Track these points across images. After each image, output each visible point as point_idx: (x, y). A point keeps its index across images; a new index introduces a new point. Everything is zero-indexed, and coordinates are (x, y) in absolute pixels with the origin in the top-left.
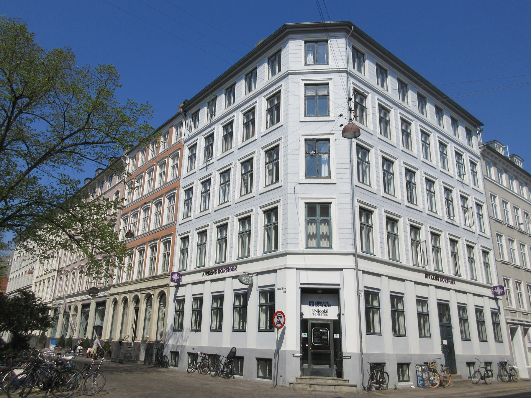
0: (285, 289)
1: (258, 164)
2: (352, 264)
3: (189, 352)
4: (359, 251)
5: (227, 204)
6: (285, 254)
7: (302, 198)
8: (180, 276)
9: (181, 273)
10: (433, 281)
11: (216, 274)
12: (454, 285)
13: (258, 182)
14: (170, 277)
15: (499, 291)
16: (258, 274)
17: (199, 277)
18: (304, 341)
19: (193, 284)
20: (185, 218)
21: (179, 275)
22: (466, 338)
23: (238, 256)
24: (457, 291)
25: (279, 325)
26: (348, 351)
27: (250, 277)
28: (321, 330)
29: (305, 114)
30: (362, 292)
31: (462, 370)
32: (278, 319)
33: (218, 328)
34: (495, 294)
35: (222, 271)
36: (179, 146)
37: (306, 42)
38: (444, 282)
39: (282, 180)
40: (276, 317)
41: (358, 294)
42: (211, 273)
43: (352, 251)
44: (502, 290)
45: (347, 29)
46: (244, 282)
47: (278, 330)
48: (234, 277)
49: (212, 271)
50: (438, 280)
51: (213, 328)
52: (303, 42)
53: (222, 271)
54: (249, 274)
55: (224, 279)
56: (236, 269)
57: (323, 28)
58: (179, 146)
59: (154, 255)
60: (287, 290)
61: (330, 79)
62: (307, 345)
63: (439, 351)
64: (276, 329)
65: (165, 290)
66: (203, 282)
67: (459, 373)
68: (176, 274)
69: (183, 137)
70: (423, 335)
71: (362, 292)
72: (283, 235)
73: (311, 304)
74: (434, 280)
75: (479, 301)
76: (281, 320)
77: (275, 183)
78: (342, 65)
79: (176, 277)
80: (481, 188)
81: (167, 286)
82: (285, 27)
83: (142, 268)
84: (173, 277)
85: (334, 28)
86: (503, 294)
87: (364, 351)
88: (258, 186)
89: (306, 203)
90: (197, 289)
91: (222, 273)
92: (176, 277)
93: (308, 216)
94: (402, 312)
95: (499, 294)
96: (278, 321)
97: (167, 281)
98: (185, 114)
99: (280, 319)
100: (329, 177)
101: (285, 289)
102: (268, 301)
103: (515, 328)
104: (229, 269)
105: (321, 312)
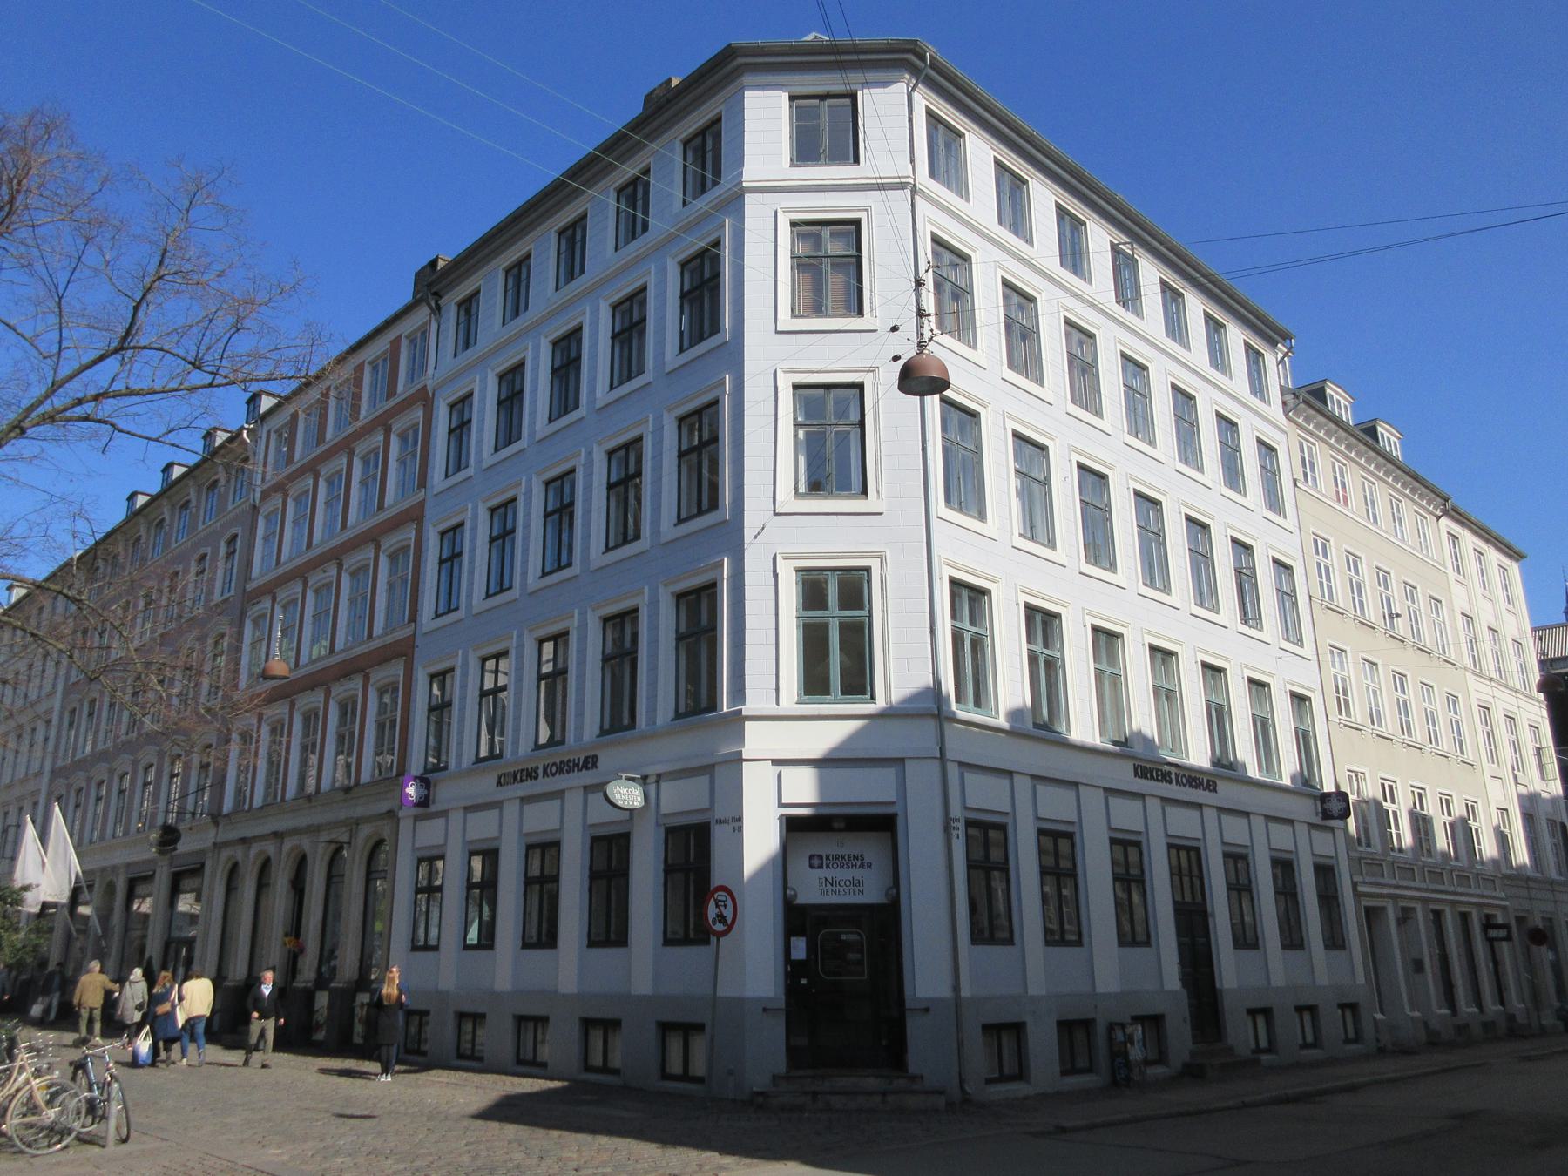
5: (565, 573)
10: (1156, 783)
11: (536, 778)
18: (793, 970)
20: (442, 615)
22: (1246, 939)
23: (601, 727)
24: (1221, 810)
25: (719, 927)
28: (844, 937)
29: (793, 310)
31: (1240, 1034)
33: (544, 938)
35: (554, 769)
37: (792, 98)
38: (1185, 786)
41: (947, 829)
47: (718, 940)
50: (1171, 782)
51: (419, 941)
52: (785, 96)
56: (595, 765)
57: (832, 58)
61: (867, 210)
62: (804, 981)
63: (1172, 978)
64: (713, 939)
73: (816, 862)
75: (1282, 838)
78: (896, 167)
82: (729, 53)
85: (862, 57)
87: (966, 992)
89: (798, 570)
90: (482, 827)
91: (554, 775)
93: (805, 608)
96: (718, 916)
99: (722, 908)
105: (842, 883)
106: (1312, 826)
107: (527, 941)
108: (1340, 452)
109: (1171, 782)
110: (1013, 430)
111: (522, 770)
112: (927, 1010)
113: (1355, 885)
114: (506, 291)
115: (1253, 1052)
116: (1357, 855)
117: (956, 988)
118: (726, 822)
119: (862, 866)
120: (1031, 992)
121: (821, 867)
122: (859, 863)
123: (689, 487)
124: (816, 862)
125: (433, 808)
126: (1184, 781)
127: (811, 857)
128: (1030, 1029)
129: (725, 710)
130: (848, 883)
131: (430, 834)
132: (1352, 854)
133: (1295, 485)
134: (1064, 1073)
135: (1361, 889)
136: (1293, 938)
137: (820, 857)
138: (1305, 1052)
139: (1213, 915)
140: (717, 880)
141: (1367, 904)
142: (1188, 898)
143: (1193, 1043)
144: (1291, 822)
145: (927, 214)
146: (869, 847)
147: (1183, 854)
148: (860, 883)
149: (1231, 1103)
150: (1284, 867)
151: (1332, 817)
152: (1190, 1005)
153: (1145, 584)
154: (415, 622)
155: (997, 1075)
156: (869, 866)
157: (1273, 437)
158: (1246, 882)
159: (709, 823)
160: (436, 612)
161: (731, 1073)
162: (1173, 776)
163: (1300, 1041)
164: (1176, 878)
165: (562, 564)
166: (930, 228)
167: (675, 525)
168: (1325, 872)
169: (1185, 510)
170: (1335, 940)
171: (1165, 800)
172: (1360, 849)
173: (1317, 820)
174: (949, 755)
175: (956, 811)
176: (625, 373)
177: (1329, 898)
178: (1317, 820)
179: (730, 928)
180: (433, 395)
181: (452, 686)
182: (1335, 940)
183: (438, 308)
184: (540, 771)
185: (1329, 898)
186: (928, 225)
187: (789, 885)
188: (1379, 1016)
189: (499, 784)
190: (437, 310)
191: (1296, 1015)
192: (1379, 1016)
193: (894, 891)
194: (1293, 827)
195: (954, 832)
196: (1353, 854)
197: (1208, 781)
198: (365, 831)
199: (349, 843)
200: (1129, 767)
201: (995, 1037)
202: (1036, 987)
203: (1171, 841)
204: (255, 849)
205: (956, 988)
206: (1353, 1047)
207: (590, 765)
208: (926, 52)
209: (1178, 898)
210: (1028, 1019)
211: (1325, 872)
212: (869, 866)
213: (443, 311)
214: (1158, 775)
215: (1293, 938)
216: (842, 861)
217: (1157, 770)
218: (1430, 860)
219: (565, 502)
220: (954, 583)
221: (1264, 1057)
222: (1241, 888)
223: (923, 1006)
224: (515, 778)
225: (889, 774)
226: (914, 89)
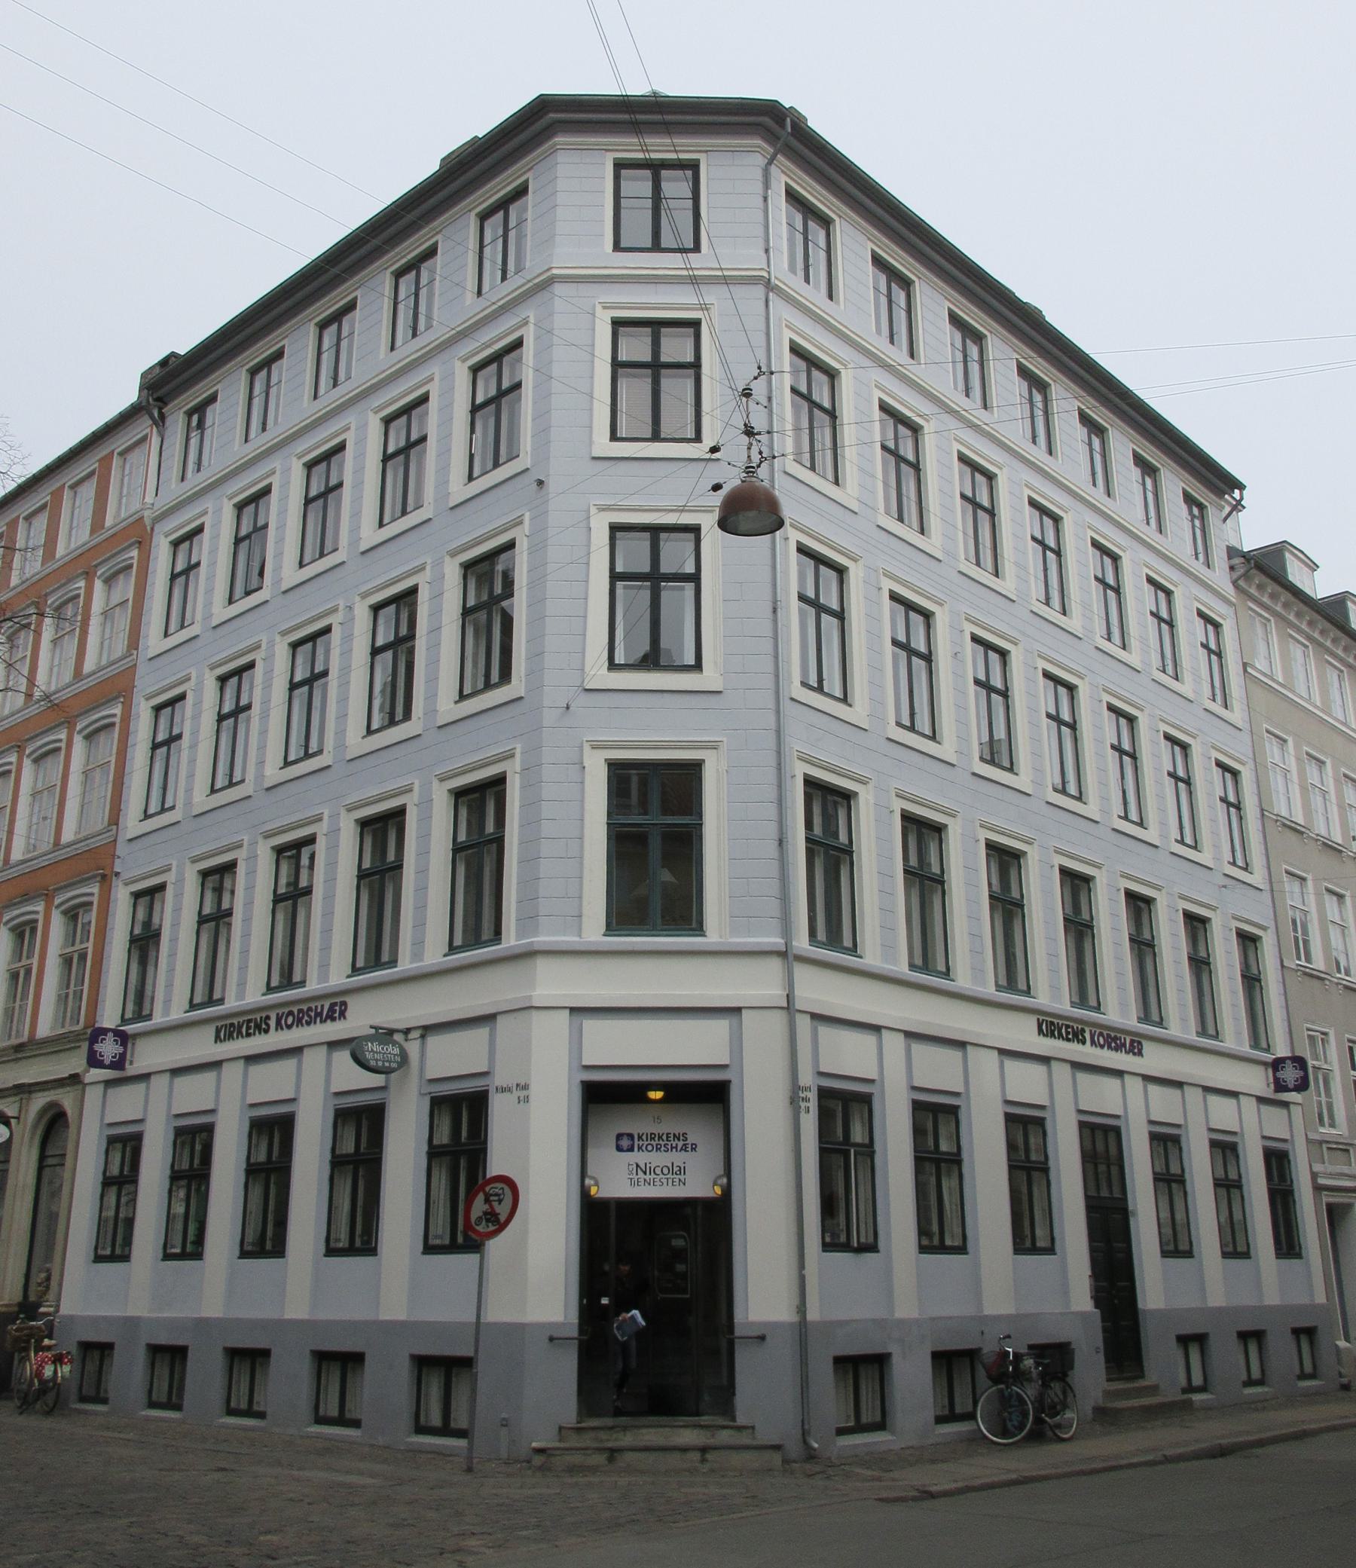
0: (526, 1087)
1: (436, 613)
2: (780, 992)
3: (154, 1342)
4: (802, 943)
6: (529, 954)
7: (596, 746)
8: (124, 1044)
9: (129, 1028)
12: (1137, 1059)
13: (433, 680)
14: (85, 1045)
15: (1290, 1074)
16: (427, 1030)
17: (202, 1046)
19: (176, 1072)
21: (123, 1038)
24: (1147, 1079)
26: (753, 1317)
27: (395, 1043)
30: (810, 1095)
32: (487, 1207)
34: (1280, 1086)
35: (290, 1020)
36: (138, 534)
38: (1102, 1047)
39: (523, 674)
40: (481, 1197)
41: (795, 1099)
42: (248, 1028)
43: (776, 941)
44: (1302, 1073)
45: (768, 130)
46: (373, 1063)
48: (333, 1045)
49: (254, 1023)
50: (1084, 1043)
53: (290, 1020)
54: (391, 1032)
55: (297, 1051)
56: (342, 1015)
58: (138, 534)
59: (24, 962)
60: (534, 1091)
62: (605, 1301)
63: (1081, 1298)
65: (66, 1099)
66: (216, 1065)
67: (1152, 1377)
68: (110, 1034)
69: (149, 499)
70: (1028, 1244)
71: (810, 1095)
72: (522, 883)
73: (625, 1143)
74: (1068, 1040)
75: (1224, 1114)
76: (498, 1208)
77: (497, 686)
78: (746, 258)
79: (108, 1049)
80: (1237, 714)
81: (75, 1079)
83: (25, 996)
84: (96, 1047)
86: (1302, 1086)
87: (813, 1315)
88: (432, 696)
91: (289, 1027)
92: (108, 1049)
94: (955, 1160)
95: (1291, 1086)
96: (485, 1213)
97: (74, 1062)
98: (160, 409)
99: (495, 1204)
100: (698, 666)
101: (526, 1087)
102: (464, 1134)
103: (1342, 1205)
104: (319, 1014)
105: (658, 1171)
106: (1261, 1100)
107: (332, 1245)
108: (1299, 631)
109: (1084, 1043)
110: (972, 633)
111: (249, 1021)
112: (762, 1338)
113: (1314, 1176)
114: (250, 398)
115: (1185, 1391)
116: (1317, 1137)
117: (802, 1309)
118: (510, 1090)
119: (684, 1148)
120: (899, 1314)
121: (631, 1149)
122: (680, 1144)
123: (475, 655)
124: (625, 1143)
125: (131, 1070)
126: (1102, 1041)
127: (619, 1137)
128: (896, 1360)
129: (513, 942)
130: (665, 1171)
131: (125, 1105)
132: (1311, 1136)
133: (1245, 671)
134: (940, 1420)
135: (1321, 1181)
136: (1235, 1247)
137: (631, 1136)
138: (1249, 1391)
139: (1134, 1214)
140: (496, 1166)
141: (1331, 1200)
142: (1105, 1193)
143: (1108, 1380)
144: (1234, 1094)
145: (785, 316)
146: (697, 1127)
147: (1099, 1136)
148: (682, 1170)
149: (1150, 1457)
150: (1225, 1148)
151: (1286, 1089)
152: (1105, 1330)
153: (982, 759)
154: (117, 824)
155: (852, 1424)
156: (694, 1148)
157: (1218, 610)
158: (1236, 1177)
159: (487, 1091)
160: (145, 811)
161: (505, 1423)
162: (1087, 1036)
163: (1297, 1371)
164: (1090, 1167)
165: (310, 752)
166: (788, 334)
167: (456, 702)
168: (1277, 1160)
169: (1107, 698)
170: (1288, 1244)
171: (1077, 1066)
172: (1322, 1130)
173: (1269, 1092)
174: (799, 1005)
175: (807, 1078)
176: (399, 507)
177: (1282, 1197)
178: (1269, 1092)
179: (502, 1227)
180: (152, 529)
181: (162, 912)
182: (1288, 1244)
183: (162, 417)
184: (272, 1023)
185: (1282, 1197)
186: (785, 330)
187: (589, 1173)
188: (1342, 1344)
189: (218, 1039)
190: (161, 421)
191: (1178, 1354)
192: (1342, 1344)
193: (725, 1180)
194: (1238, 1101)
195: (803, 1105)
196: (1312, 1136)
197: (1132, 1041)
198: (39, 1101)
199: (17, 1118)
200: (1032, 1022)
201: (851, 1376)
202: (906, 1308)
203: (1215, 1136)
204: (39, 1101)
205: (802, 1309)
206: (1259, 1390)
207: (337, 1015)
208: (786, 116)
209: (1093, 1193)
210: (893, 1349)
211: (1277, 1160)
212: (694, 1148)
213: (168, 422)
214: (1068, 1033)
215: (1235, 1247)
216: (659, 1142)
217: (1067, 1027)
218: (1333, 1131)
219: (316, 671)
220: (810, 783)
221: (1197, 1397)
222: (1229, 1186)
223: (759, 1333)
224: (240, 1033)
225: (721, 1026)
226: (770, 162)
